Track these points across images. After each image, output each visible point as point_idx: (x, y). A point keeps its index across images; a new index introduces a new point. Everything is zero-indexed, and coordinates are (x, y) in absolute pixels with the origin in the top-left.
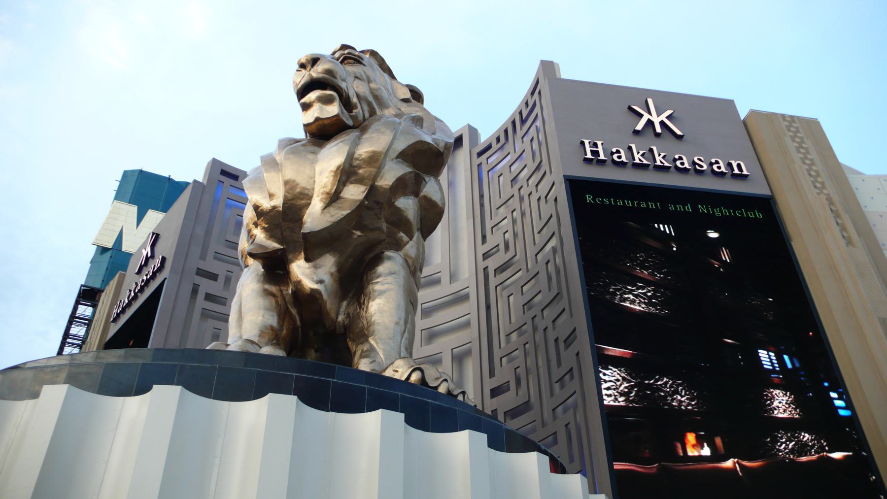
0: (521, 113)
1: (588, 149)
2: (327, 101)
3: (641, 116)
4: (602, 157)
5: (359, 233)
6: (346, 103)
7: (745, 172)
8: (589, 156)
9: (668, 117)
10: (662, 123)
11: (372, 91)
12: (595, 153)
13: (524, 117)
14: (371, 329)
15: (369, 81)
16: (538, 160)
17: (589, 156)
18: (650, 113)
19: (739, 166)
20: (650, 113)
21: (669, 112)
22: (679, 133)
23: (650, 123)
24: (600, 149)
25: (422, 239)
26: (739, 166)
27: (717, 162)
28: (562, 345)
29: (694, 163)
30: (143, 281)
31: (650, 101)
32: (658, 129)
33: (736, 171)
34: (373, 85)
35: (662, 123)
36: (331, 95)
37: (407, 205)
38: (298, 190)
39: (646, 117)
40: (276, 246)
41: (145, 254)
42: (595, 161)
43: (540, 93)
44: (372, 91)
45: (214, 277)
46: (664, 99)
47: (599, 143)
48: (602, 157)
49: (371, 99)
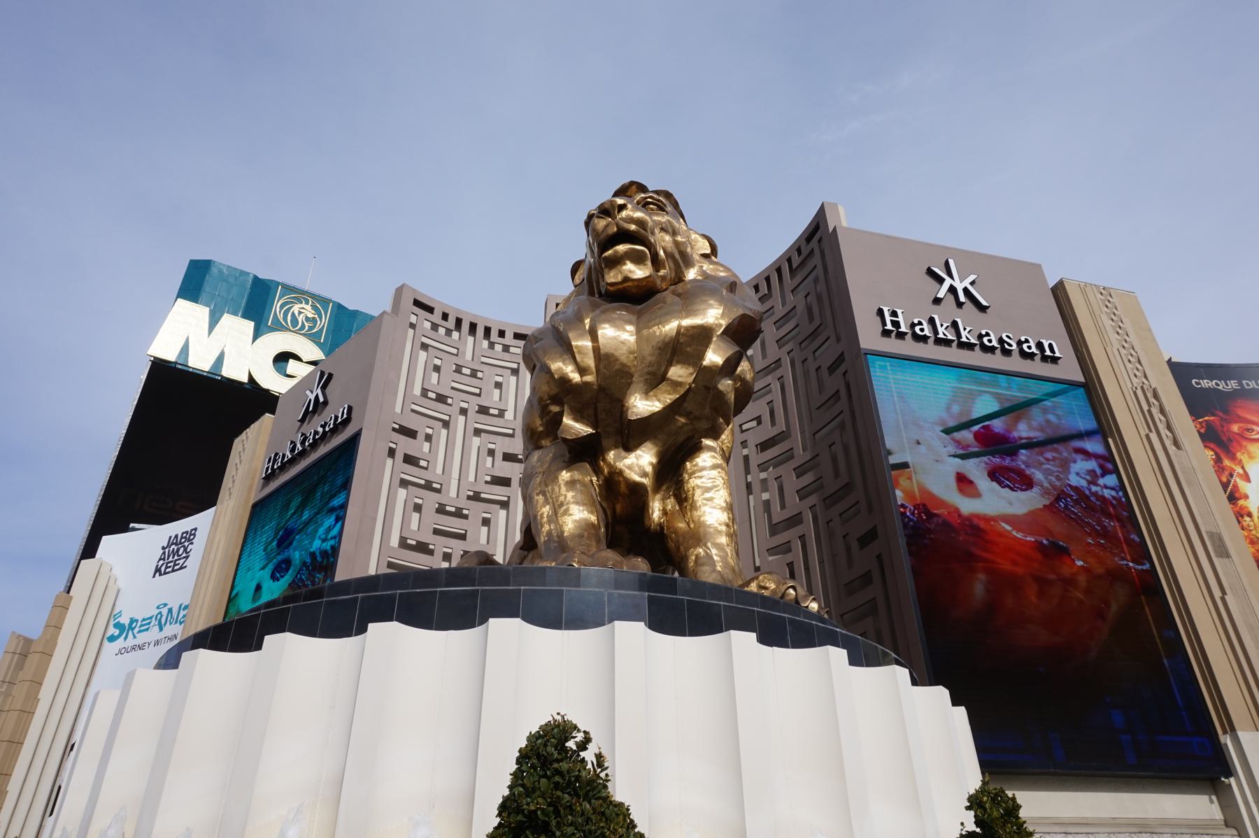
0: (789, 260)
1: (888, 318)
2: (638, 259)
3: (940, 281)
4: (903, 329)
5: (683, 420)
6: (656, 263)
7: (1057, 354)
8: (889, 327)
9: (972, 283)
10: (966, 290)
11: (676, 243)
12: (896, 324)
13: (794, 266)
14: (702, 530)
15: (674, 233)
16: (817, 322)
17: (889, 327)
18: (952, 278)
19: (1050, 346)
20: (952, 278)
21: (972, 278)
22: (984, 303)
23: (952, 290)
24: (901, 319)
25: (1226, 560)
26: (1050, 346)
27: (1027, 341)
28: (855, 545)
29: (1001, 341)
30: (316, 433)
31: (951, 262)
32: (962, 298)
33: (1048, 353)
34: (679, 238)
35: (966, 290)
36: (643, 251)
37: (726, 385)
38: (617, 367)
39: (948, 282)
40: (590, 430)
41: (312, 397)
42: (893, 335)
43: (820, 241)
44: (676, 243)
45: (411, 434)
46: (971, 260)
47: (899, 312)
48: (903, 329)
49: (677, 256)
